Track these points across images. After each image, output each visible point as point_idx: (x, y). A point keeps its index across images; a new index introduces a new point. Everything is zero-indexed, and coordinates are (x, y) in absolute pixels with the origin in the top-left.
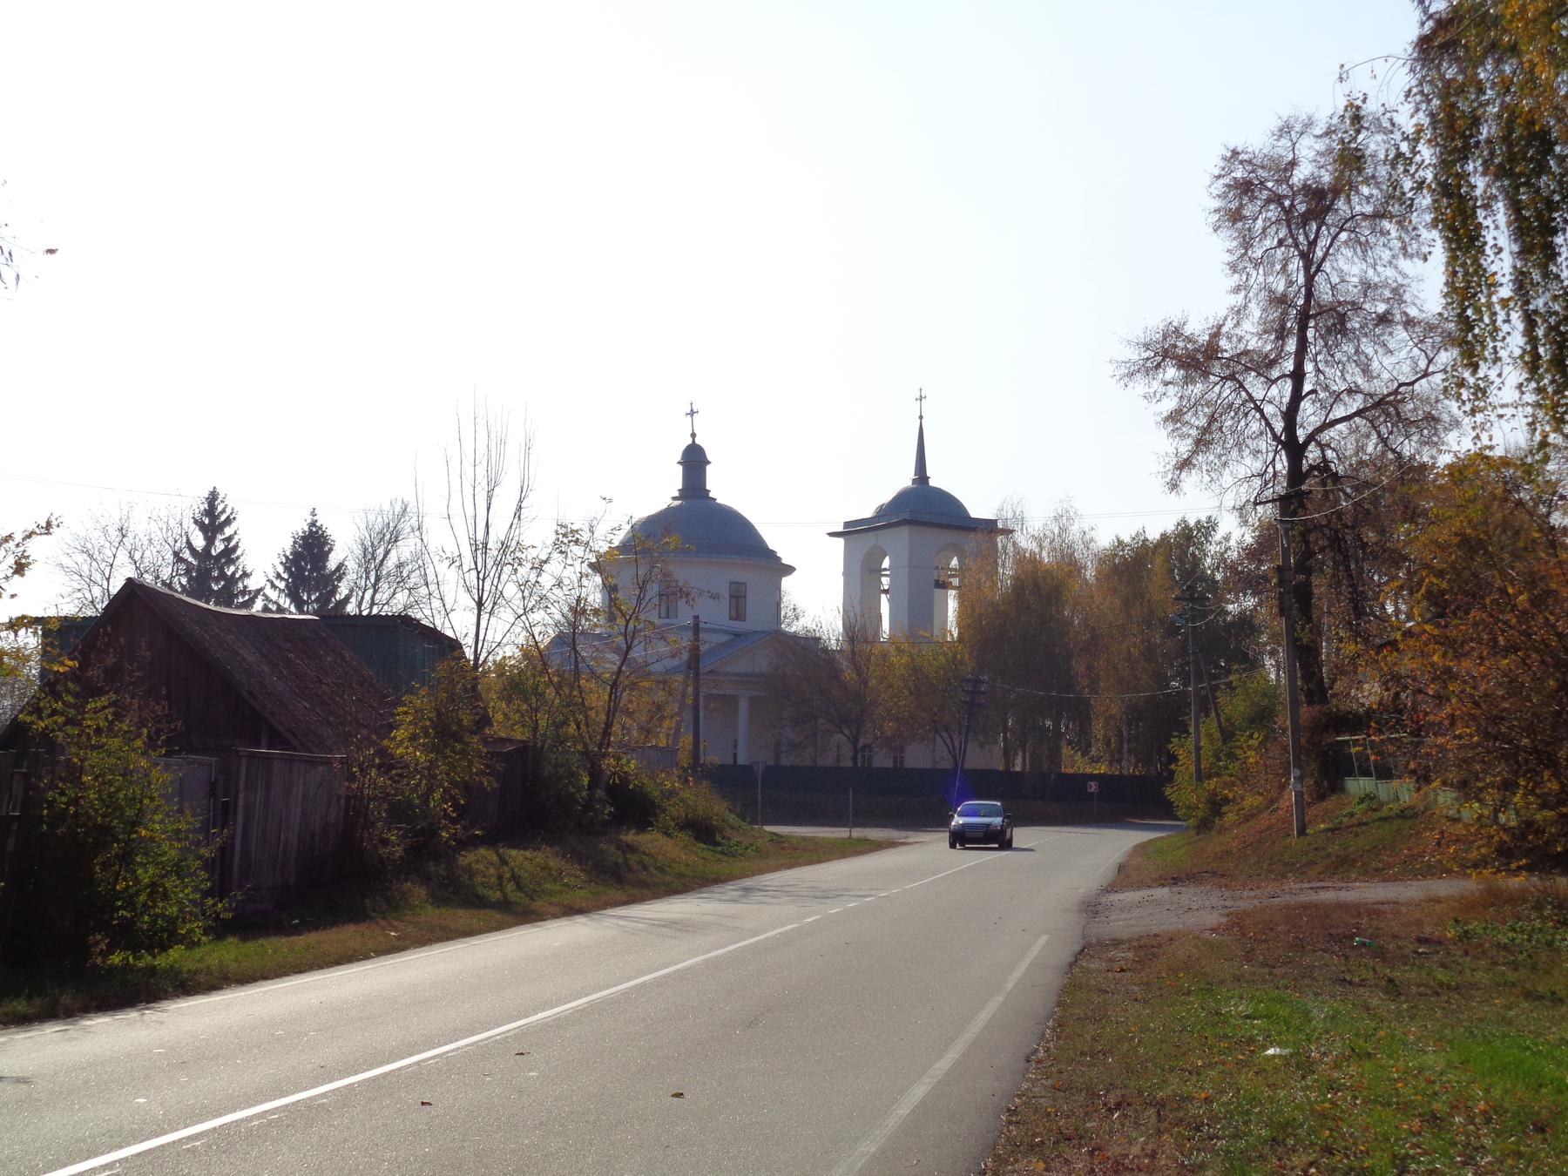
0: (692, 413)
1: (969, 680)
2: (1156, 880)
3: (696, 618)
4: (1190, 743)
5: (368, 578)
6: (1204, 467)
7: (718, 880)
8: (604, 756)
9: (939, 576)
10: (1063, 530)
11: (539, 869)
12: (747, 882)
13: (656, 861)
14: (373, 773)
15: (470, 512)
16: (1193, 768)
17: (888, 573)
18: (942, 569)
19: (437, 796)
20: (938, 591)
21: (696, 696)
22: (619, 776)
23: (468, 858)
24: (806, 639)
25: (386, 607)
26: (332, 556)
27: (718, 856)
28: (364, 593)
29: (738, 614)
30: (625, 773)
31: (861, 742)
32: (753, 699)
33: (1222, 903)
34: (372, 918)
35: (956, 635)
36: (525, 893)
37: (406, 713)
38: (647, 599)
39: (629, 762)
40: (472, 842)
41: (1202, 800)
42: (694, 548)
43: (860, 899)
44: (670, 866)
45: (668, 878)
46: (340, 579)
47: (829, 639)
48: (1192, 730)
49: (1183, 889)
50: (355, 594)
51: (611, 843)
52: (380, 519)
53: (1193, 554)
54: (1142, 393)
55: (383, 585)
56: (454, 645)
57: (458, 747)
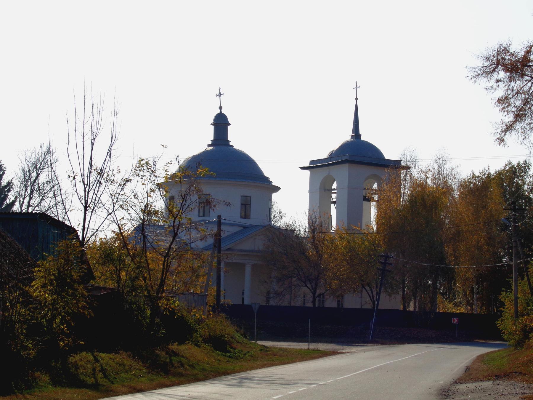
0: (220, 95)
1: (382, 256)
2: (486, 377)
3: (219, 217)
4: (512, 295)
5: (26, 190)
6: (520, 130)
7: (226, 373)
8: (160, 298)
9: (366, 194)
10: (440, 167)
11: (118, 365)
12: (243, 375)
13: (189, 361)
14: (18, 306)
15: (81, 152)
16: (513, 310)
17: (336, 191)
18: (368, 189)
19: (58, 320)
20: (365, 203)
21: (219, 263)
22: (169, 310)
23: (74, 359)
24: (286, 230)
25: (37, 208)
26: (4, 177)
27: (228, 359)
28: (24, 199)
29: (246, 215)
30: (172, 309)
31: (318, 292)
32: (254, 266)
33: (522, 391)
34: (14, 393)
35: (375, 229)
36: (109, 379)
37: (39, 271)
38: (187, 205)
39: (174, 302)
40: (78, 349)
41: (519, 329)
42: (215, 174)
43: (308, 385)
44: (198, 364)
45: (195, 372)
46: (9, 191)
47: (300, 231)
48: (513, 287)
49: (501, 382)
50: (18, 200)
51: (163, 350)
52: (34, 156)
53: (517, 183)
54: (485, 86)
55: (36, 195)
56: (72, 231)
57: (70, 291)
